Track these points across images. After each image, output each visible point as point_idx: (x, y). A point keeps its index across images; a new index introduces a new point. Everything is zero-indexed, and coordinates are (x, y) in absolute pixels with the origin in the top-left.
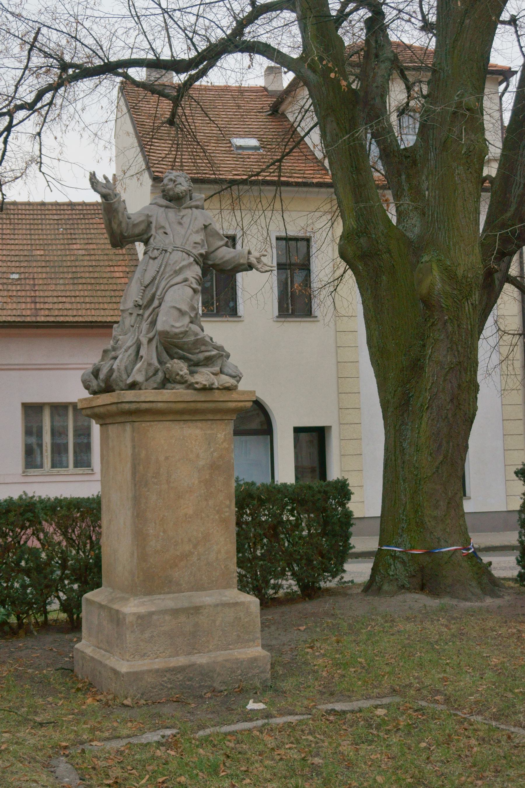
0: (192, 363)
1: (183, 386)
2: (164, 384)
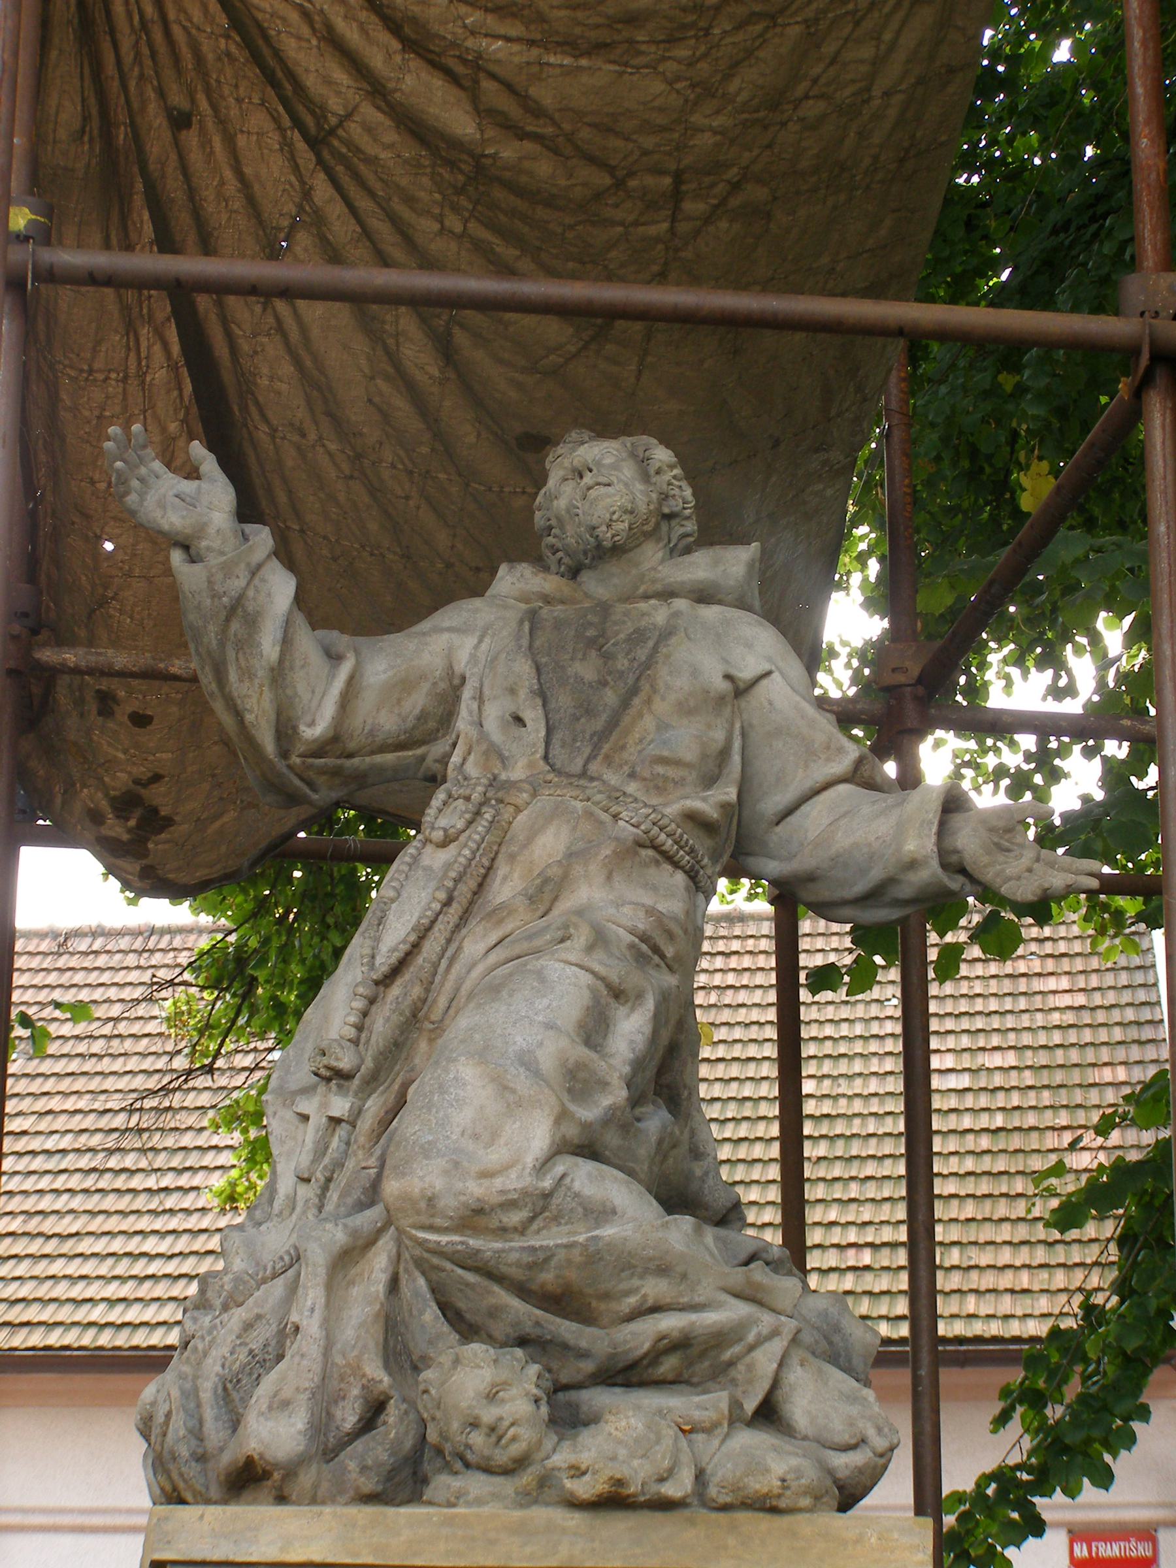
0: (588, 1366)
1: (507, 1486)
2: (405, 1481)
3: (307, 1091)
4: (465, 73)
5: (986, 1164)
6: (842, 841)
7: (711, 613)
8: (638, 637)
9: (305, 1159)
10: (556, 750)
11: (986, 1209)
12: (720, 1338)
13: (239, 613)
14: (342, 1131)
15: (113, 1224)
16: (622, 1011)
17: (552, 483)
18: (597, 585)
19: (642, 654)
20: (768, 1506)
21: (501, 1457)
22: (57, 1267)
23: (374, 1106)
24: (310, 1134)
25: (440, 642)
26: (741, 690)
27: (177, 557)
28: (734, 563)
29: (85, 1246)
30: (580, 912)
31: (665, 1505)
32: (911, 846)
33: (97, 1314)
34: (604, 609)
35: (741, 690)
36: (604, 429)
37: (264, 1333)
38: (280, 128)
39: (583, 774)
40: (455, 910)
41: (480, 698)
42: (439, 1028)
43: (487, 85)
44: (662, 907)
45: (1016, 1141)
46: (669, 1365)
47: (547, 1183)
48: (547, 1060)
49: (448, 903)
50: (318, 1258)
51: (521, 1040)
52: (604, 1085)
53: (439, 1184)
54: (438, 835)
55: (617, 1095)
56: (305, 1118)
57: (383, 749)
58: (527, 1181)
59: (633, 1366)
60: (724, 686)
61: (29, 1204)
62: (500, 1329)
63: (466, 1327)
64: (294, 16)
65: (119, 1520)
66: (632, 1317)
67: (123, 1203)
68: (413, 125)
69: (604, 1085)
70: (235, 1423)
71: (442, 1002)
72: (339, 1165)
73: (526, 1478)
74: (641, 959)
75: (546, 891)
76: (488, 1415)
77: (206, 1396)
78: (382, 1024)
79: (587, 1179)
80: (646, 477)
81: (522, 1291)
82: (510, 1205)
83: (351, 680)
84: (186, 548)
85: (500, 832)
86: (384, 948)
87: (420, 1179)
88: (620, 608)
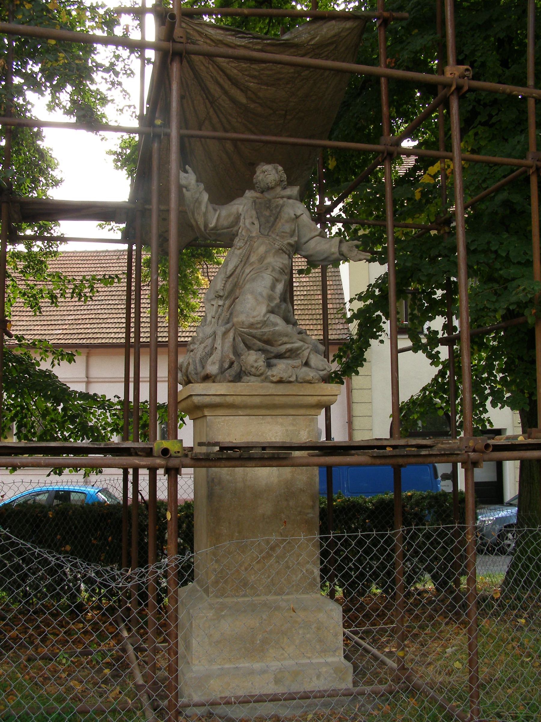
0: (273, 355)
1: (259, 379)
2: (238, 378)
3: (212, 299)
4: (244, 90)
5: (303, 302)
6: (318, 248)
7: (291, 201)
8: (277, 206)
9: (214, 314)
10: (262, 230)
11: (303, 312)
12: (298, 349)
13: (198, 202)
14: (221, 308)
15: (114, 316)
16: (277, 284)
17: (258, 173)
18: (268, 195)
19: (278, 210)
20: (309, 382)
21: (258, 373)
22: (103, 325)
23: (228, 303)
24: (214, 308)
25: (236, 207)
26: (297, 217)
27: (184, 190)
28: (295, 190)
29: (109, 321)
30: (269, 263)
31: (290, 382)
32: (333, 250)
33: (112, 335)
34: (270, 201)
35: (297, 217)
36: (268, 162)
37: (208, 349)
38: (203, 99)
39: (268, 235)
40: (243, 263)
41: (244, 219)
42: (241, 288)
43: (249, 92)
44: (284, 262)
45: (309, 297)
46: (287, 354)
47: (265, 319)
48: (265, 294)
49: (241, 261)
50: (219, 334)
51: (259, 290)
52: (275, 299)
53: (245, 319)
54: (238, 247)
55: (277, 301)
56: (213, 305)
57: (224, 229)
58: (262, 318)
59: (281, 355)
60: (294, 217)
61: (96, 312)
62: (255, 348)
63: (249, 348)
64: (209, 77)
65: (107, 380)
66: (280, 345)
67: (116, 311)
68: (233, 100)
69: (275, 299)
70: (203, 367)
71: (241, 282)
72: (221, 315)
73: (263, 377)
74: (281, 273)
75: (262, 259)
76: (256, 365)
77: (197, 361)
78: (229, 287)
79: (274, 318)
80: (277, 173)
81: (260, 340)
82: (258, 323)
83: (219, 215)
84: (186, 188)
85: (251, 247)
86: (228, 270)
87: (241, 318)
88: (273, 200)
